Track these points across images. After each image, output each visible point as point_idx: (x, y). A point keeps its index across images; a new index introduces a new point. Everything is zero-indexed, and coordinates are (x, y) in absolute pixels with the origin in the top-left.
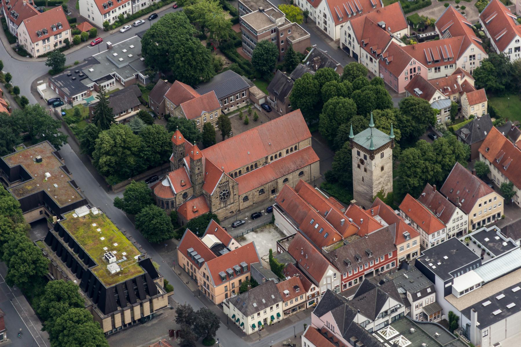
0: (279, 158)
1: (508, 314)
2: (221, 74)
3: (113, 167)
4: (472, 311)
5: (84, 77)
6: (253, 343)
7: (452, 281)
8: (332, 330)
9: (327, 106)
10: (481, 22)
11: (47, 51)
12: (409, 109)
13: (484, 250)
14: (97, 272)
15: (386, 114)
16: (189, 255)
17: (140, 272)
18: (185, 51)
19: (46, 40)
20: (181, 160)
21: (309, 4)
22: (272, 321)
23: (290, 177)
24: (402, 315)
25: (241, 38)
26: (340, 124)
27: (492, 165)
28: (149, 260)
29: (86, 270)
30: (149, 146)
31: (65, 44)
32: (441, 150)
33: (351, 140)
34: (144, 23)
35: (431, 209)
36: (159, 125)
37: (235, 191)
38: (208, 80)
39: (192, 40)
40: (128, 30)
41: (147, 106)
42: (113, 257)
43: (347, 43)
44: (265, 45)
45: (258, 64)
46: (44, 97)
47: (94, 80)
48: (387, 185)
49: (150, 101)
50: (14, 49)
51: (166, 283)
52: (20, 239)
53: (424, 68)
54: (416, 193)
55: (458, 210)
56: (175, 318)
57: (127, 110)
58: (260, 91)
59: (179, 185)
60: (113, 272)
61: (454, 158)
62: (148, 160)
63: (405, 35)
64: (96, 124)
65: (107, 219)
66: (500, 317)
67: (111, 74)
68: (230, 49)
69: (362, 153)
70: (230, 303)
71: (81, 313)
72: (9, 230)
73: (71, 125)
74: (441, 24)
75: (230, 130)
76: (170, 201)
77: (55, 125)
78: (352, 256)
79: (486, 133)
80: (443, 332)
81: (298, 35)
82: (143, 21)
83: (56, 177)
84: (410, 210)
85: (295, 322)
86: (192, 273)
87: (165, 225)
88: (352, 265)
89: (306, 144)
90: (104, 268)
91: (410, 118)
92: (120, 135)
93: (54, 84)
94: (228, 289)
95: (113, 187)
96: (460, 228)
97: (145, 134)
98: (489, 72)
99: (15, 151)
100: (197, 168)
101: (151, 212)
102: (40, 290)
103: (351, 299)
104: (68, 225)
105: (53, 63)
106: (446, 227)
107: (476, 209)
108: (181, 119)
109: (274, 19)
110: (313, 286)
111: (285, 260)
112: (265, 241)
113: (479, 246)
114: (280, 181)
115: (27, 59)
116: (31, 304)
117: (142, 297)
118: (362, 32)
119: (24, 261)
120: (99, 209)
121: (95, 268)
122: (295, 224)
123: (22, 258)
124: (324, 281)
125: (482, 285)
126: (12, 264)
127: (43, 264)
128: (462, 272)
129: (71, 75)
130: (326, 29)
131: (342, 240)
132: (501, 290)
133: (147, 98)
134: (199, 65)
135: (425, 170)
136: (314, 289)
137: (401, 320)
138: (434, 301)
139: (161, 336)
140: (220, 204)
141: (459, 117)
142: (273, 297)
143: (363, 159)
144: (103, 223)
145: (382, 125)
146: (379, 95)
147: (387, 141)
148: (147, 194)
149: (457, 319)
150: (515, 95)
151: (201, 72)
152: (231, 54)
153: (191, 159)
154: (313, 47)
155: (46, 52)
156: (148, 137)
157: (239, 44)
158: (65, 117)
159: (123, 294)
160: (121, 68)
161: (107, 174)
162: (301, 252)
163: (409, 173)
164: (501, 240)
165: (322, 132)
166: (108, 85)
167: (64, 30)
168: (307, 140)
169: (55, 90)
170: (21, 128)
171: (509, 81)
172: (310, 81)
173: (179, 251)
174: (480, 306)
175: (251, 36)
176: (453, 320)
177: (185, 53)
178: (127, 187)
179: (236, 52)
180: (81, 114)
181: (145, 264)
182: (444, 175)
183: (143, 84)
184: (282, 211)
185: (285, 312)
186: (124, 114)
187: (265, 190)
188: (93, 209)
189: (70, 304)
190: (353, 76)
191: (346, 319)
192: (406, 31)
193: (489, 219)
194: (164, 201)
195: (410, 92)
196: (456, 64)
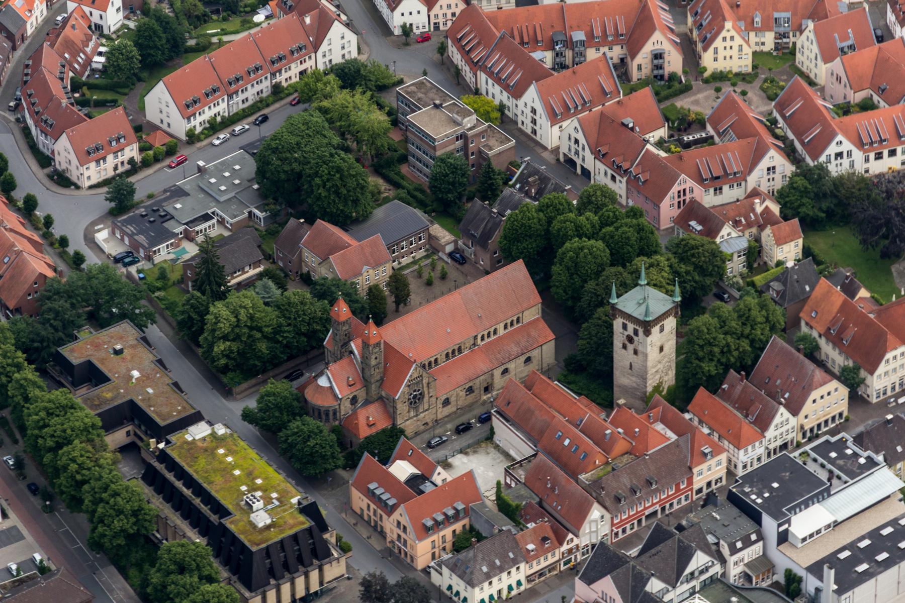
0: (493, 338)
2: (383, 207)
3: (233, 359)
4: (825, 567)
5: (168, 217)
7: (789, 521)
9: (564, 253)
10: (776, 114)
11: (103, 178)
12: (689, 254)
13: (831, 472)
14: (236, 526)
15: (656, 263)
16: (370, 494)
17: (303, 523)
18: (329, 173)
19: (101, 161)
20: (346, 344)
21: (505, 94)
22: (509, 592)
24: (714, 578)
25: (407, 149)
26: (585, 281)
27: (823, 337)
28: (315, 502)
29: (217, 524)
30: (289, 325)
31: (130, 166)
32: (749, 317)
33: (613, 306)
34: (248, 130)
35: (737, 409)
36: (296, 292)
37: (431, 390)
38: (364, 218)
39: (339, 156)
40: (225, 141)
41: (271, 261)
42: (258, 501)
43: (573, 153)
45: (440, 190)
46: (106, 250)
47: (183, 222)
48: (667, 374)
49: (277, 254)
50: (50, 177)
51: (339, 539)
52: (110, 476)
53: (698, 190)
54: (713, 385)
55: (782, 409)
56: (358, 594)
57: (243, 269)
58: (445, 232)
59: (345, 383)
60: (261, 525)
61: (768, 328)
62: (287, 346)
63: (661, 137)
64: (203, 293)
65: (240, 441)
66: (867, 576)
67: (209, 212)
68: (390, 167)
69: (631, 327)
70: (443, 567)
71: (222, 591)
72: (89, 464)
73: (157, 294)
74: (716, 120)
75: (408, 295)
76: (331, 409)
77: (138, 295)
78: (626, 487)
79: (807, 288)
81: (496, 143)
82: (247, 127)
83: (148, 378)
84: (706, 413)
85: (544, 594)
86: (376, 522)
87: (328, 448)
88: (627, 501)
89: (533, 313)
90: (245, 519)
91: (690, 268)
92: (245, 307)
93: (122, 231)
94: (437, 546)
95: (234, 389)
96: (784, 437)
97: (283, 305)
98: (801, 192)
99: (76, 338)
100: (373, 357)
101: (305, 429)
102: (138, 556)
103: (636, 554)
104: (180, 453)
105: (116, 197)
106: (765, 437)
108: (333, 279)
109: (459, 119)
110: (570, 536)
111: (521, 497)
112: (481, 468)
113: (823, 466)
114: (497, 373)
115: (71, 191)
116: (126, 577)
117: (306, 561)
118: (596, 135)
119: (120, 512)
120: (226, 426)
121: (232, 519)
122: (530, 440)
123: (116, 507)
124: (586, 528)
125: (834, 526)
126: (99, 517)
127: (149, 515)
128: (803, 507)
129: (146, 215)
130: (534, 132)
131: (607, 463)
133: (272, 247)
134: (351, 193)
135: (725, 349)
136: (572, 540)
138: (761, 554)
140: (409, 412)
141: (759, 264)
142: (511, 555)
143: (632, 334)
144: (234, 447)
145: (652, 280)
146: (643, 234)
147: (669, 306)
148: (294, 400)
149: (800, 580)
150: (841, 227)
151: (354, 205)
152: (392, 175)
153: (363, 342)
154: (525, 162)
155: (100, 180)
156: (287, 311)
157: (404, 159)
158: (144, 281)
160: (225, 201)
161: (225, 370)
162: (547, 484)
163: (701, 354)
164: (856, 455)
165: (557, 293)
167: (127, 145)
168: (534, 308)
169: (122, 240)
170: (83, 301)
171: (832, 206)
172: (532, 215)
174: (835, 559)
176: (794, 583)
177: (329, 177)
178: (263, 390)
179: (400, 172)
180: (169, 276)
181: (310, 510)
182: (753, 355)
183: (260, 225)
184: (507, 421)
185: (529, 579)
186: (238, 274)
187: (475, 388)
188: (216, 426)
189: (201, 578)
190: (596, 204)
191: (634, 587)
192: (662, 133)
193: (826, 422)
194: (322, 409)
195: (681, 227)
196: (746, 181)
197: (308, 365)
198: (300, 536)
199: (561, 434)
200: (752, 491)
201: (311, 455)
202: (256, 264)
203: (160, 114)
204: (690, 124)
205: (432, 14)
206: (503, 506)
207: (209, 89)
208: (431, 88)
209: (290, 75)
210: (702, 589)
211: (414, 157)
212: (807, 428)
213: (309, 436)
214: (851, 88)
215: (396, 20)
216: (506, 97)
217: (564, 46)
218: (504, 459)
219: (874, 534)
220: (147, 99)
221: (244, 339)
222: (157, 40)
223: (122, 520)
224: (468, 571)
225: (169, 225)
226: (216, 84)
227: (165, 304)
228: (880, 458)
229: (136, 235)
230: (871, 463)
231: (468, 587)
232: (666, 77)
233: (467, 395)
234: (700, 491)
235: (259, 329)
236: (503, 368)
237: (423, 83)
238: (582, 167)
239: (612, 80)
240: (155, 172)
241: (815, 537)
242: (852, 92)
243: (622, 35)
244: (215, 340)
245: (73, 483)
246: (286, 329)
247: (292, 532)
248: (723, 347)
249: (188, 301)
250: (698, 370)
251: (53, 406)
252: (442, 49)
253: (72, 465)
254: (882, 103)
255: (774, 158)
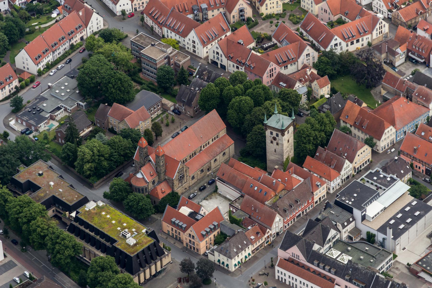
0: (208, 146)
1: (409, 227)
4: (388, 229)
6: (237, 277)
7: (365, 211)
8: (297, 258)
11: (5, 96)
14: (121, 246)
17: (151, 241)
18: (115, 81)
21: (178, 36)
23: (218, 158)
26: (245, 115)
27: (352, 127)
30: (116, 152)
34: (64, 66)
37: (187, 173)
40: (55, 73)
41: (93, 124)
42: (128, 233)
44: (164, 69)
56: (179, 269)
57: (83, 130)
58: (168, 101)
59: (149, 175)
60: (132, 244)
63: (253, 47)
67: (59, 106)
69: (275, 133)
70: (215, 252)
71: (126, 277)
76: (144, 188)
78: (287, 205)
80: (370, 247)
81: (182, 59)
82: (63, 65)
83: (58, 185)
85: (261, 257)
86: (176, 236)
87: (148, 205)
89: (223, 133)
91: (288, 103)
93: (21, 119)
94: (208, 243)
98: (325, 63)
100: (161, 162)
107: (356, 159)
109: (165, 49)
111: (240, 216)
113: (372, 184)
114: (212, 161)
116: (69, 277)
118: (226, 49)
119: (67, 247)
123: (65, 245)
124: (274, 226)
125: (384, 210)
127: (80, 247)
128: (369, 203)
129: (31, 111)
130: (195, 51)
132: (397, 211)
134: (126, 89)
135: (315, 138)
136: (269, 232)
137: (338, 243)
139: (172, 283)
140: (179, 184)
141: (312, 98)
142: (245, 242)
149: (374, 236)
150: (343, 77)
152: (137, 78)
155: (4, 97)
156: (114, 146)
159: (142, 257)
161: (89, 177)
162: (252, 208)
163: (305, 141)
166: (59, 114)
167: (14, 80)
169: (22, 123)
171: (339, 68)
173: (163, 222)
174: (388, 225)
175: (151, 64)
181: (152, 235)
184: (224, 182)
185: (253, 252)
186: (81, 132)
188: (98, 202)
193: (363, 164)
194: (140, 188)
195: (276, 86)
196: (298, 61)
197: (124, 169)
198: (151, 247)
199: (252, 185)
200: (345, 199)
201: (141, 210)
202: (89, 127)
203: (23, 64)
204: (263, 39)
205: (133, 4)
206: (233, 220)
207: (44, 50)
208: (146, 38)
209: (76, 40)
210: (333, 246)
211: (145, 69)
212: (356, 168)
213: (139, 201)
214: (332, 15)
215: (118, 9)
216: (178, 37)
217: (198, 11)
218: (225, 200)
219: (402, 211)
220: (16, 58)
221: (97, 161)
222: (14, 30)
223: (69, 251)
224: (228, 252)
225: (43, 114)
226: (47, 48)
227: (51, 150)
228: (395, 177)
229: (29, 120)
230: (393, 180)
231: (229, 259)
232: (246, 20)
233: (201, 173)
234: (316, 202)
235: (103, 156)
236: (215, 159)
237: (141, 36)
238: (221, 64)
239: (226, 24)
240: (27, 91)
241: (377, 216)
242: (333, 16)
243: (223, 3)
244: (83, 163)
245: (39, 237)
246: (115, 154)
247: (147, 245)
248: (314, 137)
249: (66, 147)
250: (304, 148)
251: (22, 203)
252: (142, 19)
253: (38, 229)
254: (347, 20)
255: (309, 50)
